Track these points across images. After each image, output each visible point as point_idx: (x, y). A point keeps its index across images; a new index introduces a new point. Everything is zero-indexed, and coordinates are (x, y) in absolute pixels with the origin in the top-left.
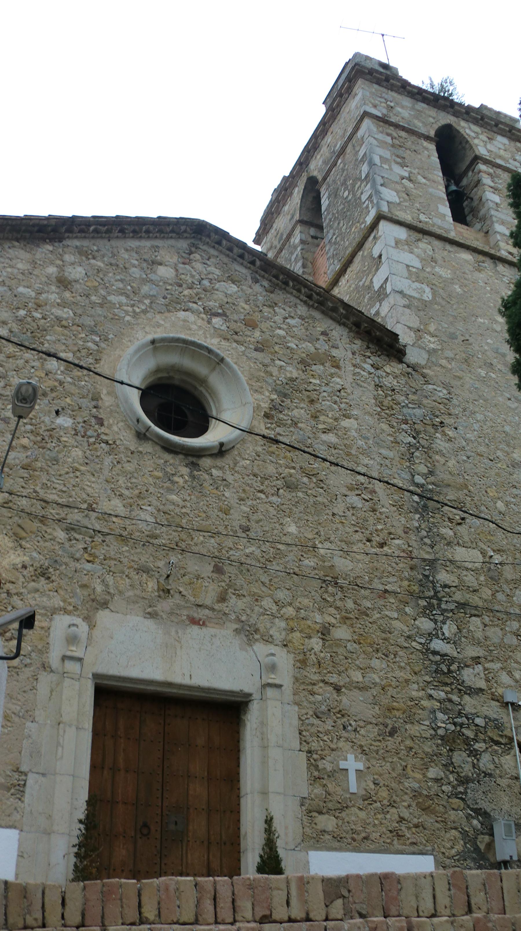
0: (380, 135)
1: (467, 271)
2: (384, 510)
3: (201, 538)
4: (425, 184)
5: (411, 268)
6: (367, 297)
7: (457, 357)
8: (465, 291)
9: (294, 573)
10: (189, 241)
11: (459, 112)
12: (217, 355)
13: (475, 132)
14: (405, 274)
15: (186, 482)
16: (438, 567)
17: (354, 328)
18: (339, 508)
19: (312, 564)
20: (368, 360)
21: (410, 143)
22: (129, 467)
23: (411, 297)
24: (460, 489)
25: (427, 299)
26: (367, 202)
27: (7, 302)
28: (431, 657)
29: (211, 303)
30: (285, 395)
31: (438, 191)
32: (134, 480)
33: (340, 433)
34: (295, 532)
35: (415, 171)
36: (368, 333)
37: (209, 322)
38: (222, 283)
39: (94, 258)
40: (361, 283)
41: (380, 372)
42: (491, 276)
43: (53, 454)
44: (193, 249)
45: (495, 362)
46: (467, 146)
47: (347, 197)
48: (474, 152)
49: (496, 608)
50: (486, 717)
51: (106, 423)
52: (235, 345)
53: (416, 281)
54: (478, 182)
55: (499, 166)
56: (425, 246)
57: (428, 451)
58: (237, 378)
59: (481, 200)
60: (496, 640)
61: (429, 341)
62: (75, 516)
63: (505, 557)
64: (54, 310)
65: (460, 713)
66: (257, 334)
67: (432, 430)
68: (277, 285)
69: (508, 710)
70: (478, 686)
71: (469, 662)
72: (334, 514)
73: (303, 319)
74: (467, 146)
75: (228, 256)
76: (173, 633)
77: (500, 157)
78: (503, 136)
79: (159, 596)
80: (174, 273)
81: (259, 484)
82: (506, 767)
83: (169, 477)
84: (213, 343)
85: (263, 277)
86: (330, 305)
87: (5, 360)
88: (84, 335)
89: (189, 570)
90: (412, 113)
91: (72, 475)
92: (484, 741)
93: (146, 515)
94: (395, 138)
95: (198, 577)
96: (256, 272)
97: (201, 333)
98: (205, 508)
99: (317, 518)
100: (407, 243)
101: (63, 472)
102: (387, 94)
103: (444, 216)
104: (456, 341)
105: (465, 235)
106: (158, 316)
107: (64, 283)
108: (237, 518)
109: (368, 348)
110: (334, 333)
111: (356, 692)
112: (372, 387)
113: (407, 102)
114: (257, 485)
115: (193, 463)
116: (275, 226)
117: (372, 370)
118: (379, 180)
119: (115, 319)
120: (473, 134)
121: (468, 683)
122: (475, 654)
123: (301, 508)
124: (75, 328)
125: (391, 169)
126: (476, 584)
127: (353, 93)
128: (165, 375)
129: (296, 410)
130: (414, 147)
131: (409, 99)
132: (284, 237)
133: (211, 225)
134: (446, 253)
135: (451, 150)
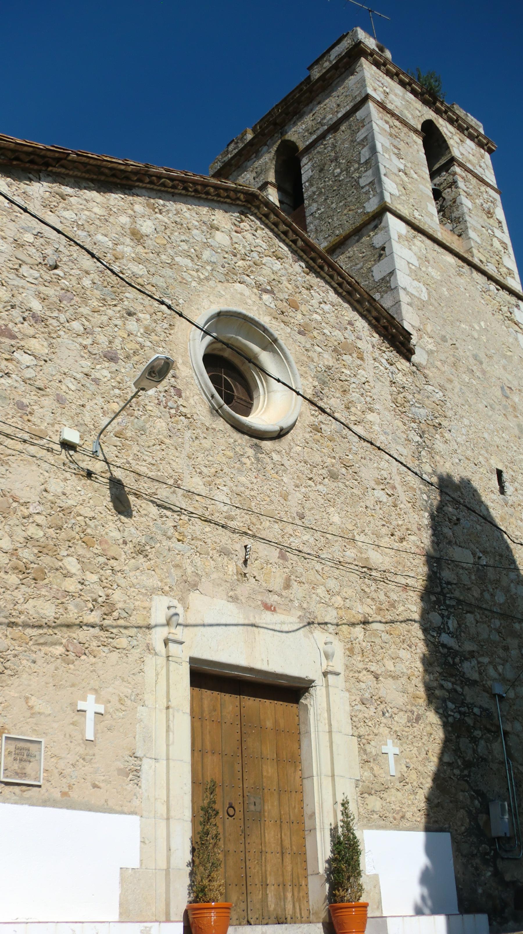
1: (452, 276)
2: (402, 506)
4: (416, 180)
12: (271, 335)
23: (412, 294)
26: (367, 188)
29: (261, 278)
32: (210, 458)
33: (367, 426)
35: (409, 165)
37: (261, 299)
41: (393, 368)
45: (475, 368)
50: (480, 707)
51: (183, 395)
52: (282, 325)
57: (431, 451)
59: (454, 202)
62: (163, 493)
75: (272, 230)
81: (309, 471)
84: (265, 320)
87: (91, 314)
89: (260, 555)
91: (158, 447)
95: (267, 562)
97: (255, 308)
98: (268, 492)
102: (383, 78)
107: (137, 236)
111: (390, 681)
119: (183, 283)
121: (468, 675)
129: (333, 399)
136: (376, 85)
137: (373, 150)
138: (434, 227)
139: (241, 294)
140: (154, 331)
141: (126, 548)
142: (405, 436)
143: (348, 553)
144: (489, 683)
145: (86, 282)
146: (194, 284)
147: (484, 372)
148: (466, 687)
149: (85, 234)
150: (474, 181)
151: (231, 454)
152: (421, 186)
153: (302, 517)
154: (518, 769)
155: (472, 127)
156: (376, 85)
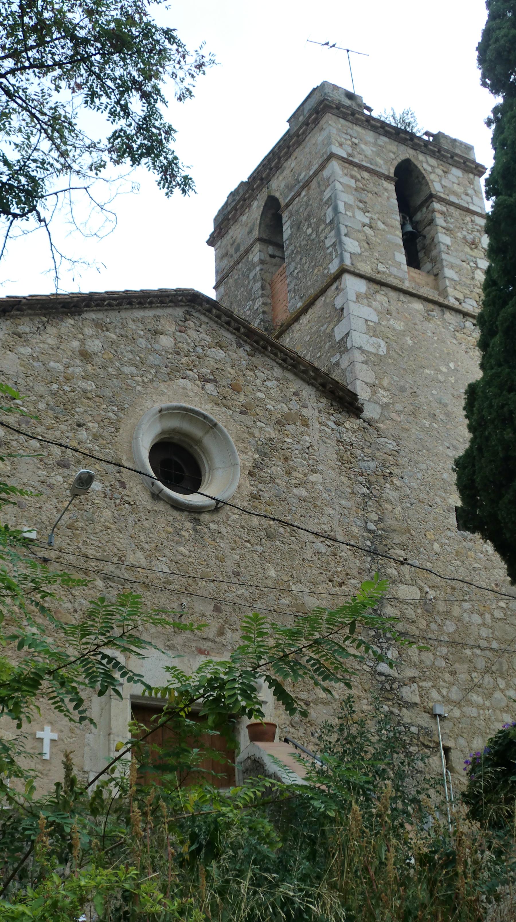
0: (345, 177)
1: (418, 322)
2: (342, 554)
3: (204, 583)
4: (384, 231)
5: (369, 323)
6: (328, 344)
7: (406, 409)
8: (415, 343)
9: (274, 610)
10: (183, 309)
11: (418, 145)
12: (211, 421)
13: (432, 166)
14: (364, 329)
15: (190, 535)
16: (385, 601)
17: (320, 388)
18: (308, 554)
19: (288, 602)
20: (331, 417)
21: (372, 184)
22: (147, 524)
23: (368, 352)
24: (403, 533)
25: (382, 354)
26: (331, 249)
27: (42, 377)
28: (378, 678)
29: (203, 370)
30: (265, 455)
31: (394, 237)
32: (151, 536)
33: (309, 487)
34: (274, 575)
35: (375, 217)
36: (332, 392)
37: (203, 389)
38: (213, 350)
39: (107, 330)
40: (322, 329)
41: (341, 428)
42: (439, 325)
43: (89, 515)
44: (188, 317)
45: (437, 412)
46: (424, 181)
47: (310, 235)
48: (429, 188)
49: (430, 636)
50: (418, 726)
51: (127, 486)
52: (224, 409)
53: (374, 336)
54: (432, 221)
55: (452, 204)
56: (382, 298)
57: (379, 500)
58: (228, 442)
60: (429, 663)
61: (383, 396)
62: (110, 568)
63: (438, 592)
64: (80, 383)
65: (399, 723)
66: (242, 398)
67: (383, 481)
68: (257, 349)
69: (436, 720)
70: (413, 701)
71: (407, 681)
72: (304, 559)
73: (278, 381)
74: (424, 181)
75: (216, 322)
76: (186, 662)
77: (455, 193)
78: (458, 168)
79: (175, 632)
80: (173, 342)
81: (246, 535)
82: (433, 765)
83: (177, 532)
84: (206, 408)
85: (245, 341)
86: (302, 368)
87: (45, 431)
88: (105, 406)
89: (196, 610)
90: (374, 149)
91: (104, 532)
92: (417, 745)
93: (163, 566)
94: (359, 180)
95: (203, 616)
96: (240, 337)
97: (197, 399)
98: (206, 557)
99: (290, 563)
100: (367, 296)
101: (98, 531)
102: (352, 129)
103: (400, 263)
104: (405, 394)
105: (417, 280)
106: (162, 385)
107: (85, 356)
108: (230, 565)
109: (332, 405)
110: (304, 393)
111: (321, 706)
112: (334, 443)
113: (369, 136)
114: (245, 536)
115: (195, 518)
116: (231, 232)
117: (335, 427)
118: (343, 230)
119: (129, 389)
120: (429, 169)
121: (406, 699)
122: (411, 675)
123: (279, 555)
124: (97, 399)
125: (354, 217)
126: (414, 616)
127: (320, 125)
128: (167, 436)
129: (274, 468)
130: (375, 190)
131: (371, 133)
132: (242, 249)
133: (203, 296)
134: (400, 304)
135: (407, 183)
136: (343, 140)
137: (336, 210)
138: (401, 276)
139: (184, 388)
140: (101, 436)
141: (76, 616)
142: (350, 490)
143: (283, 601)
144: (431, 704)
145: (42, 406)
146: (139, 388)
147: (447, 415)
148: (404, 710)
149: (41, 364)
150: (456, 213)
151: (171, 530)
152: (389, 236)
153: (237, 574)
154: (459, 780)
155: (457, 155)
156: (343, 140)
